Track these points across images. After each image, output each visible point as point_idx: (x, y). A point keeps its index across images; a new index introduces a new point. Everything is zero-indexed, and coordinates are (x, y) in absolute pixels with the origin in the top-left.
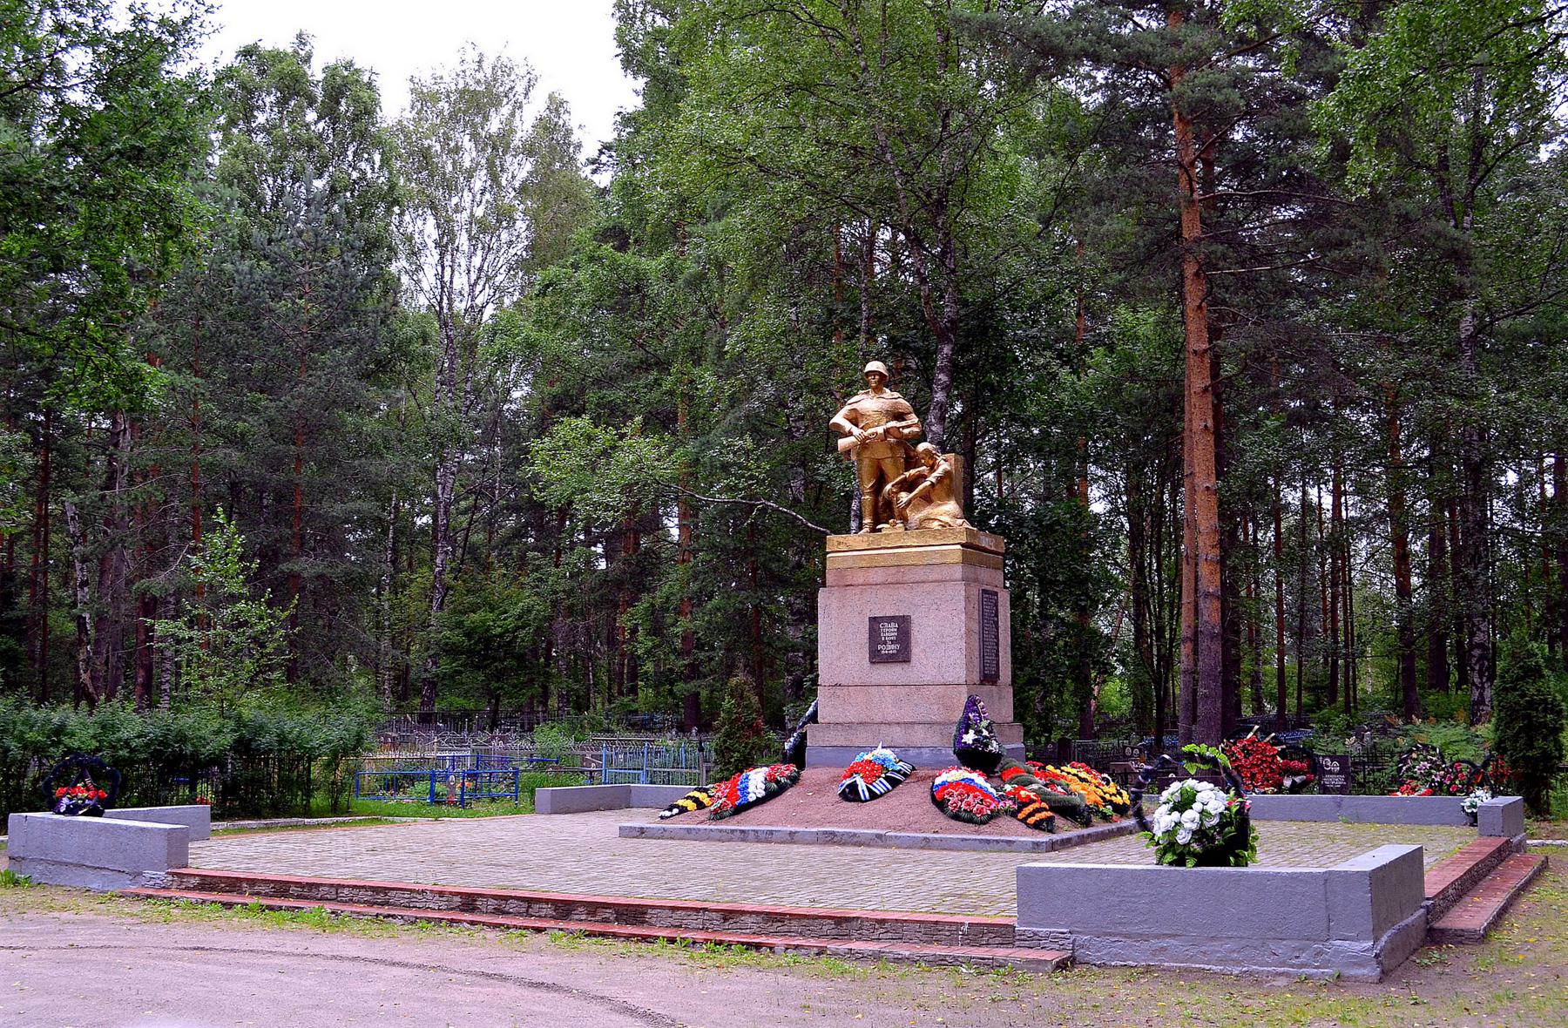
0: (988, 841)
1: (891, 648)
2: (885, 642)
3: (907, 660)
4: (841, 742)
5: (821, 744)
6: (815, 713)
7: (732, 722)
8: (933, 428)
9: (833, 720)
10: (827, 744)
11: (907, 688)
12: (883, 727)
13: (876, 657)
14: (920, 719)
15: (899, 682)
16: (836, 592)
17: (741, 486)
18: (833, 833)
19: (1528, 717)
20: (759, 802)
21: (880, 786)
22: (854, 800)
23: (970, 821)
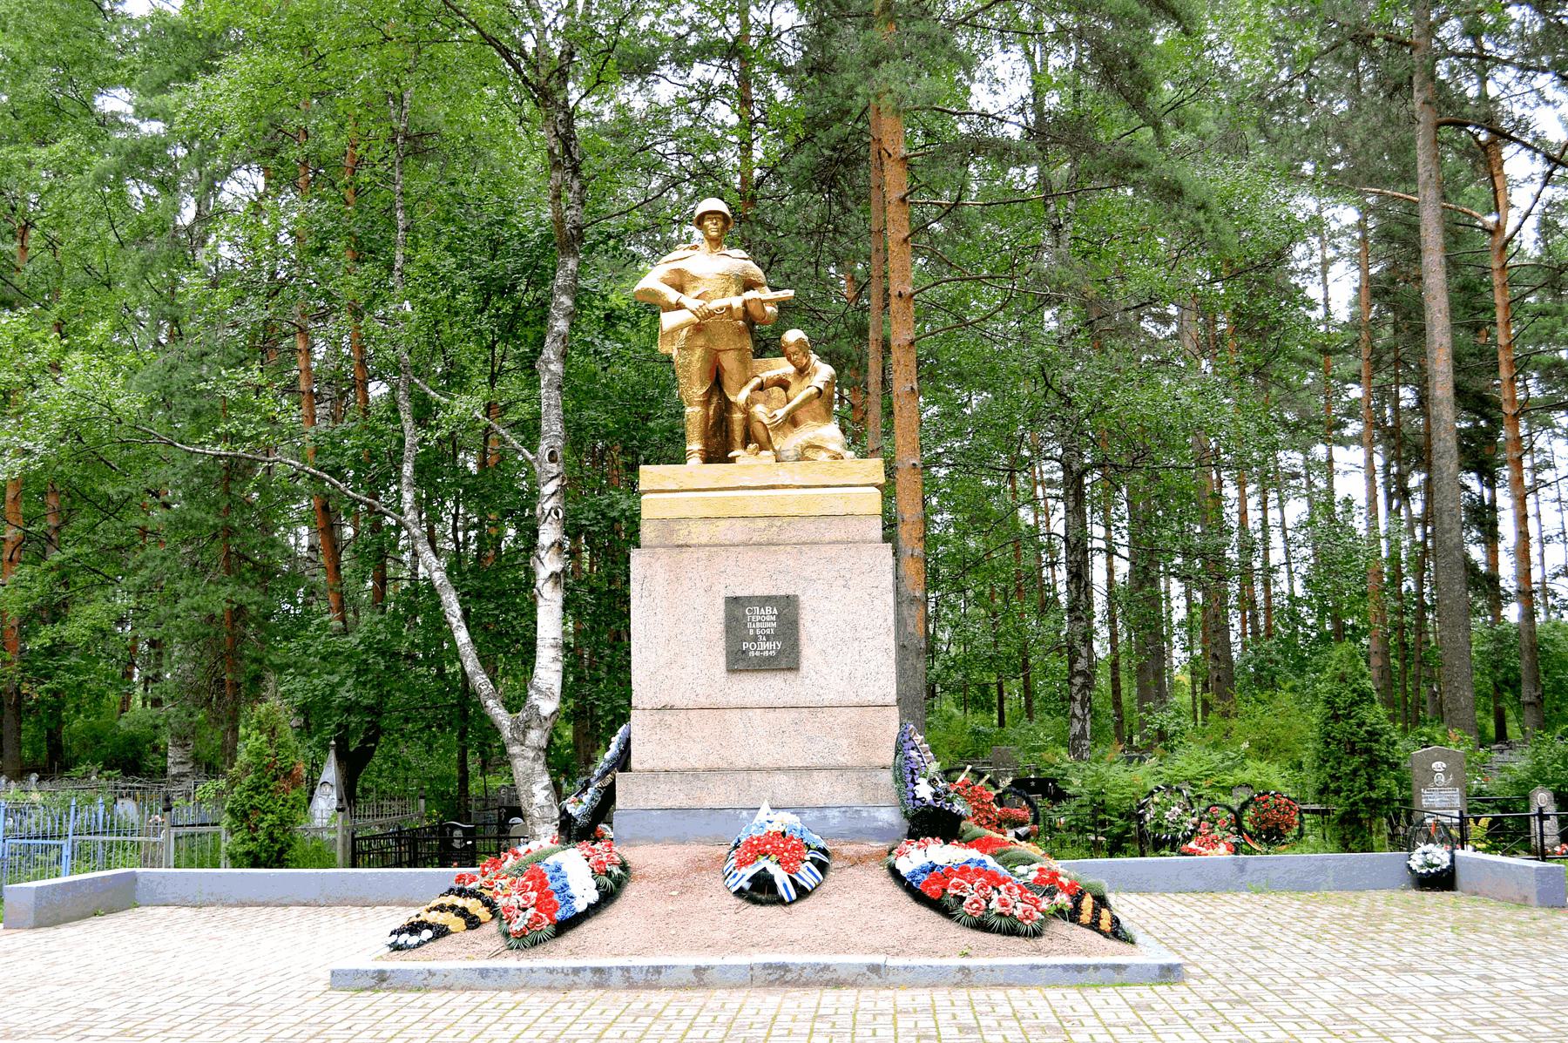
0: (1079, 968)
1: (768, 648)
2: (755, 638)
3: (794, 667)
4: (680, 800)
5: (642, 805)
6: (626, 751)
7: (262, 769)
8: (552, 367)
9: (659, 765)
10: (654, 805)
11: (794, 713)
12: (756, 776)
13: (739, 661)
14: (817, 761)
15: (780, 703)
16: (664, 556)
17: (246, 434)
18: (784, 968)
19: (1368, 751)
20: (593, 910)
21: (807, 875)
22: (773, 903)
23: (1012, 931)
